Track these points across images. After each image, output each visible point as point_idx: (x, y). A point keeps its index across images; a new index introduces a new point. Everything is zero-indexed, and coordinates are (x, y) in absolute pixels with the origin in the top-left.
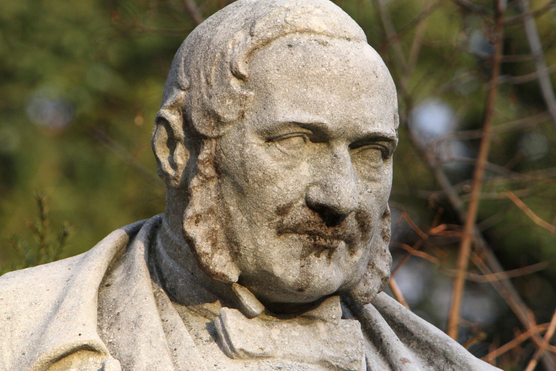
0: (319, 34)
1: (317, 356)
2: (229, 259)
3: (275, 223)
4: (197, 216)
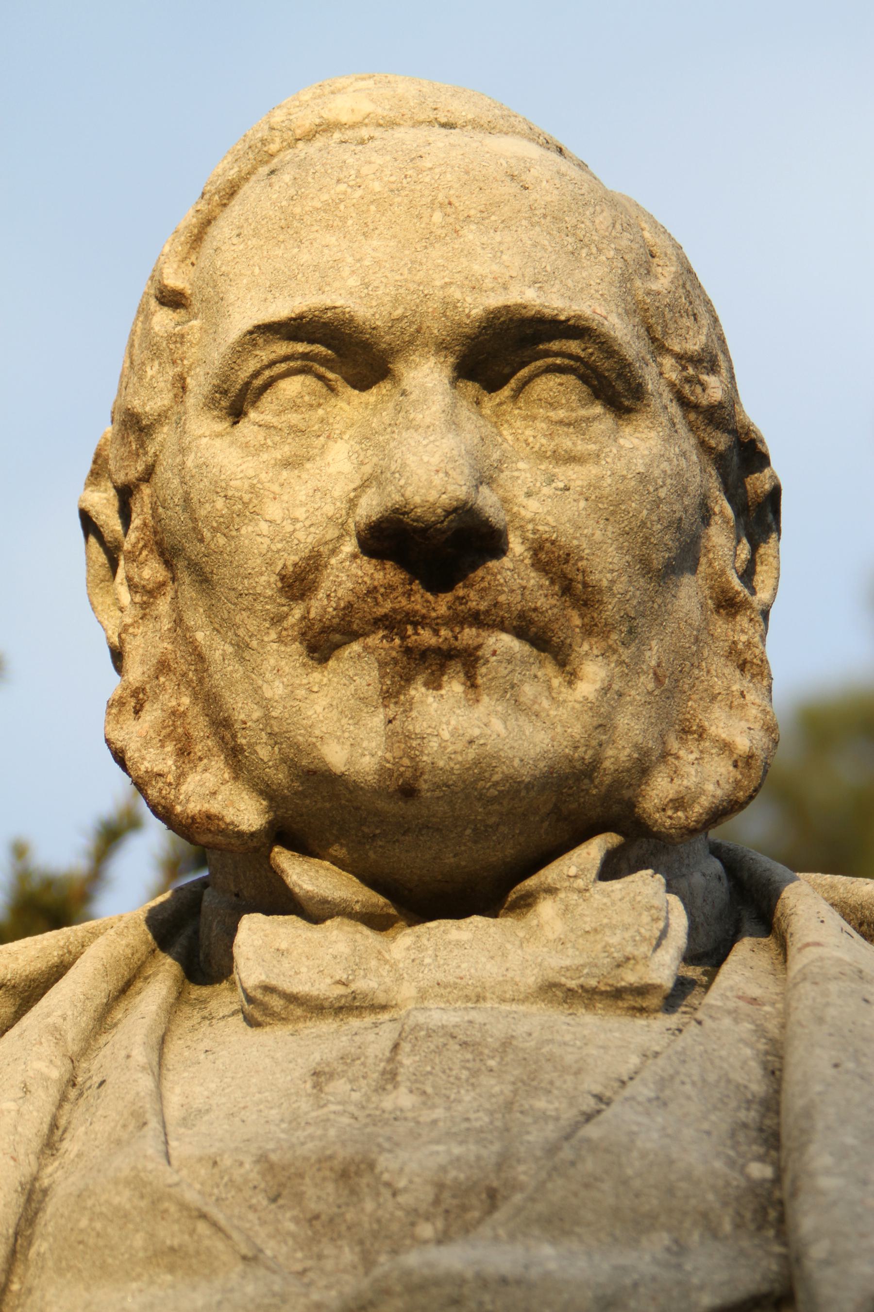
0: (353, 126)
1: (531, 979)
2: (226, 776)
3: (293, 626)
4: (135, 693)
